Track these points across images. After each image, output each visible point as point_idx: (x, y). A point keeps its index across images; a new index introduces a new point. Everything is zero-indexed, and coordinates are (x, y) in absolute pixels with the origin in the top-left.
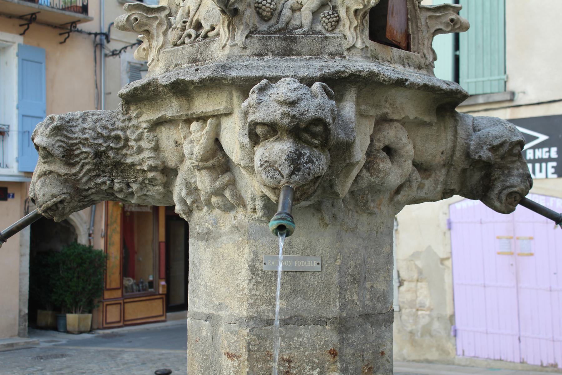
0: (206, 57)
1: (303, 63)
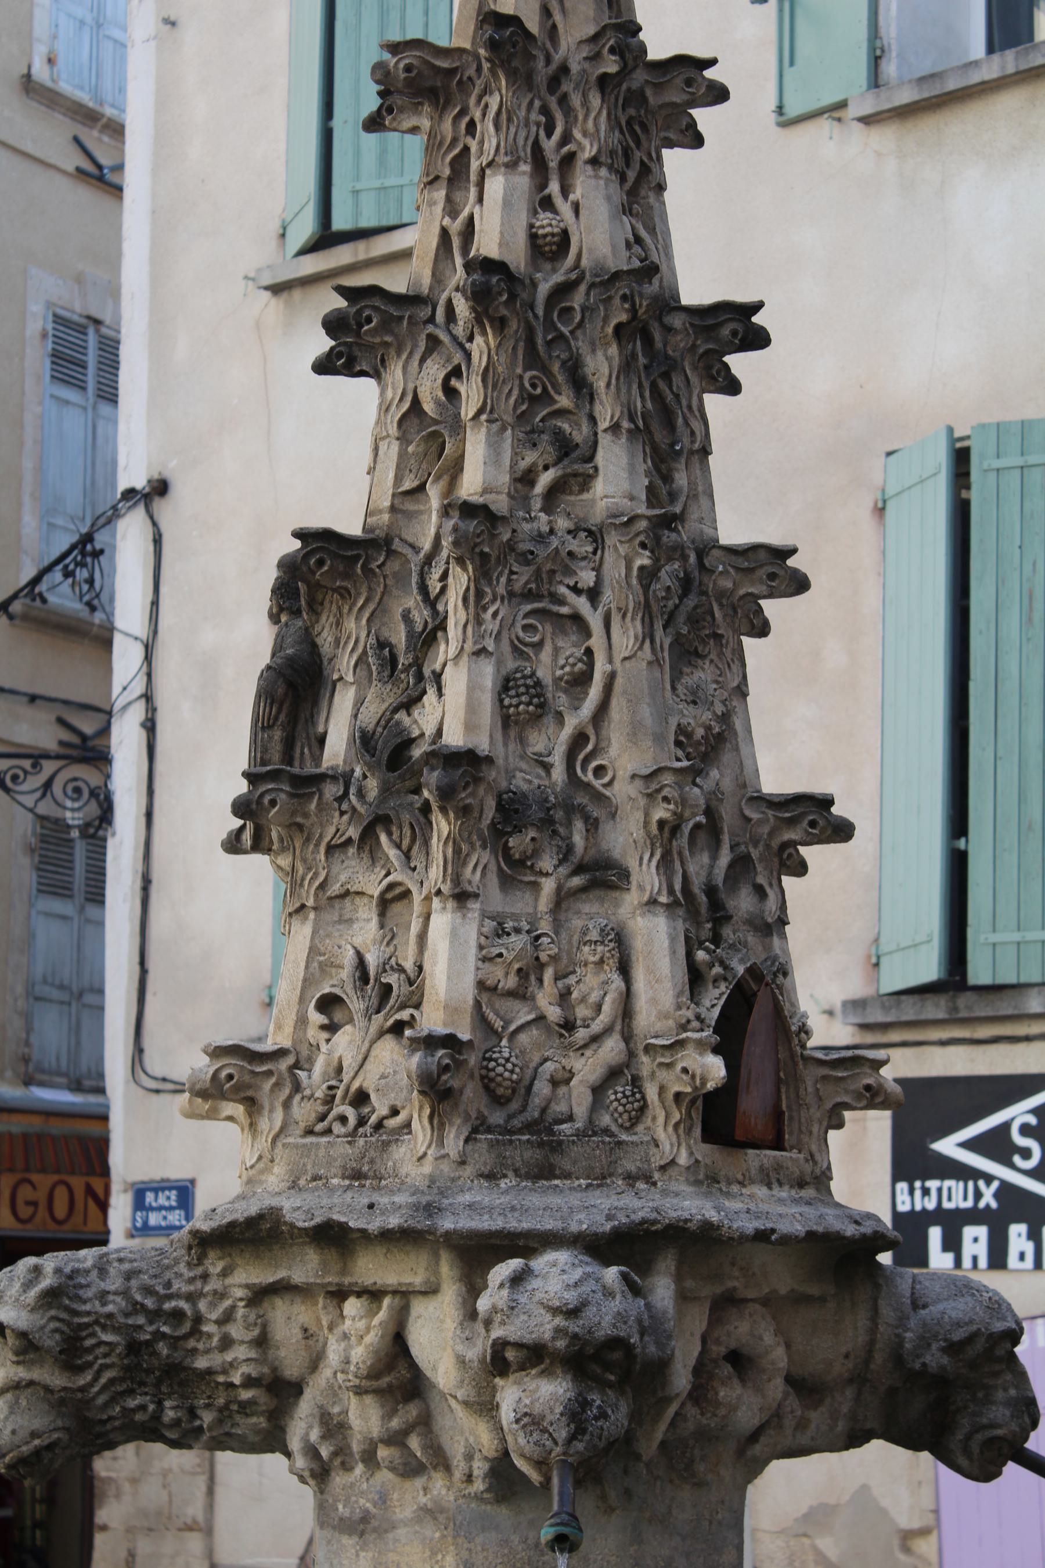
1: (575, 1200)
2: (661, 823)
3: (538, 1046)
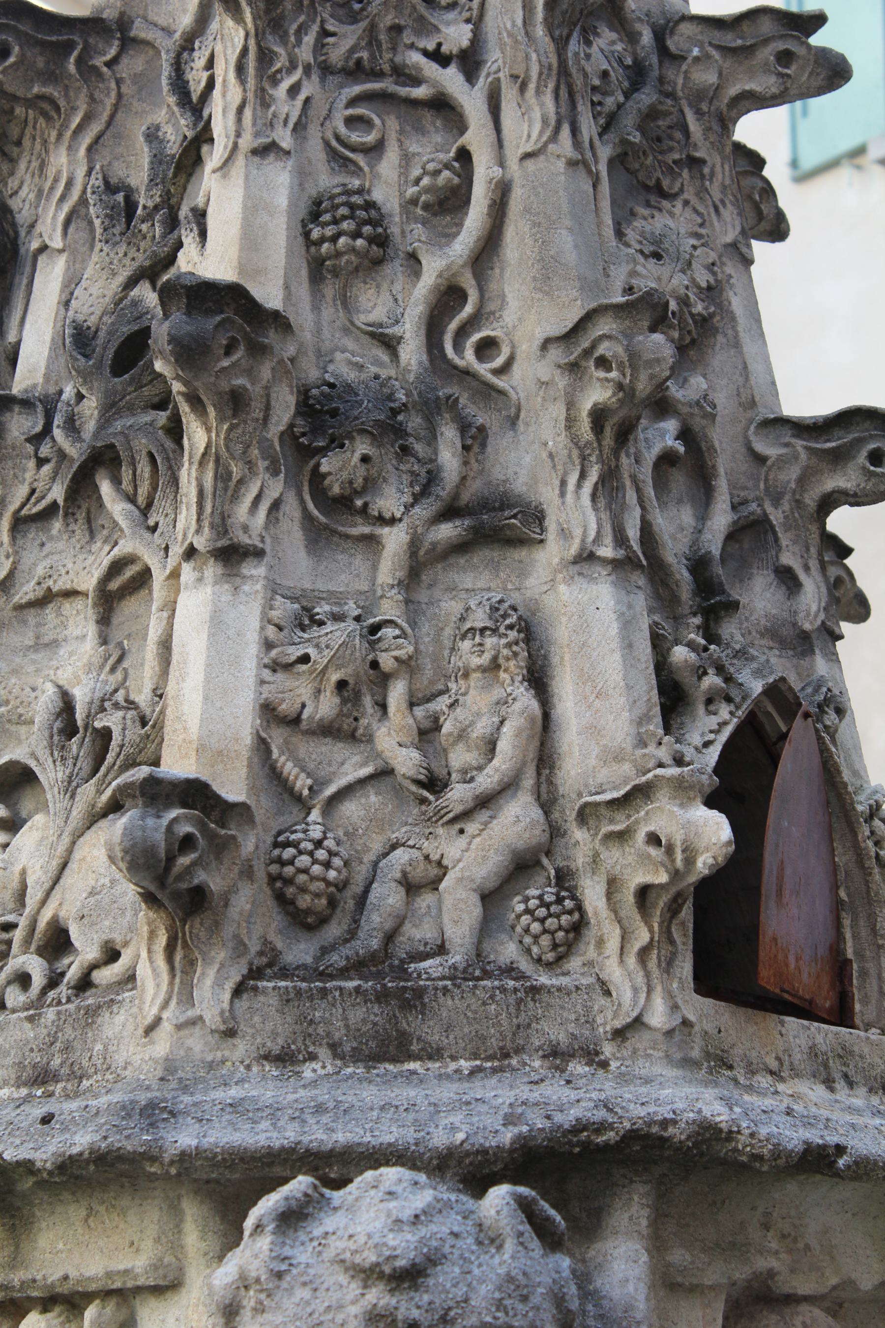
0: (85, 1063)
1: (447, 1092)
2: (599, 416)
3: (378, 823)
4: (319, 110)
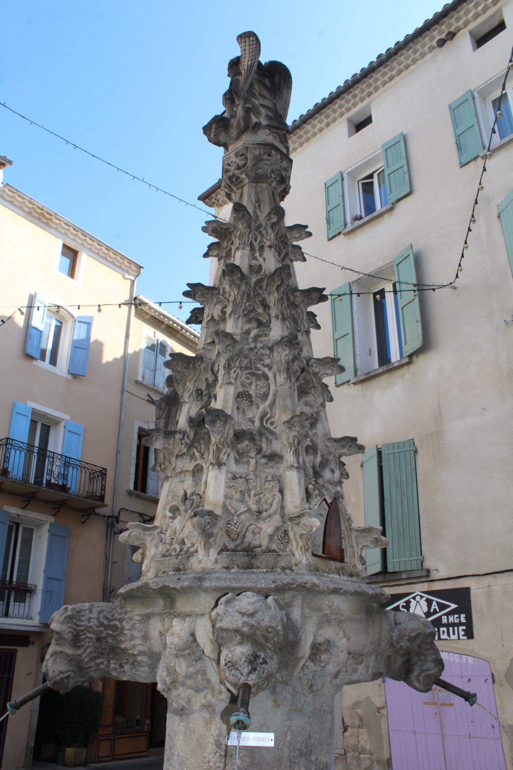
1: (261, 576)
4: (239, 376)
